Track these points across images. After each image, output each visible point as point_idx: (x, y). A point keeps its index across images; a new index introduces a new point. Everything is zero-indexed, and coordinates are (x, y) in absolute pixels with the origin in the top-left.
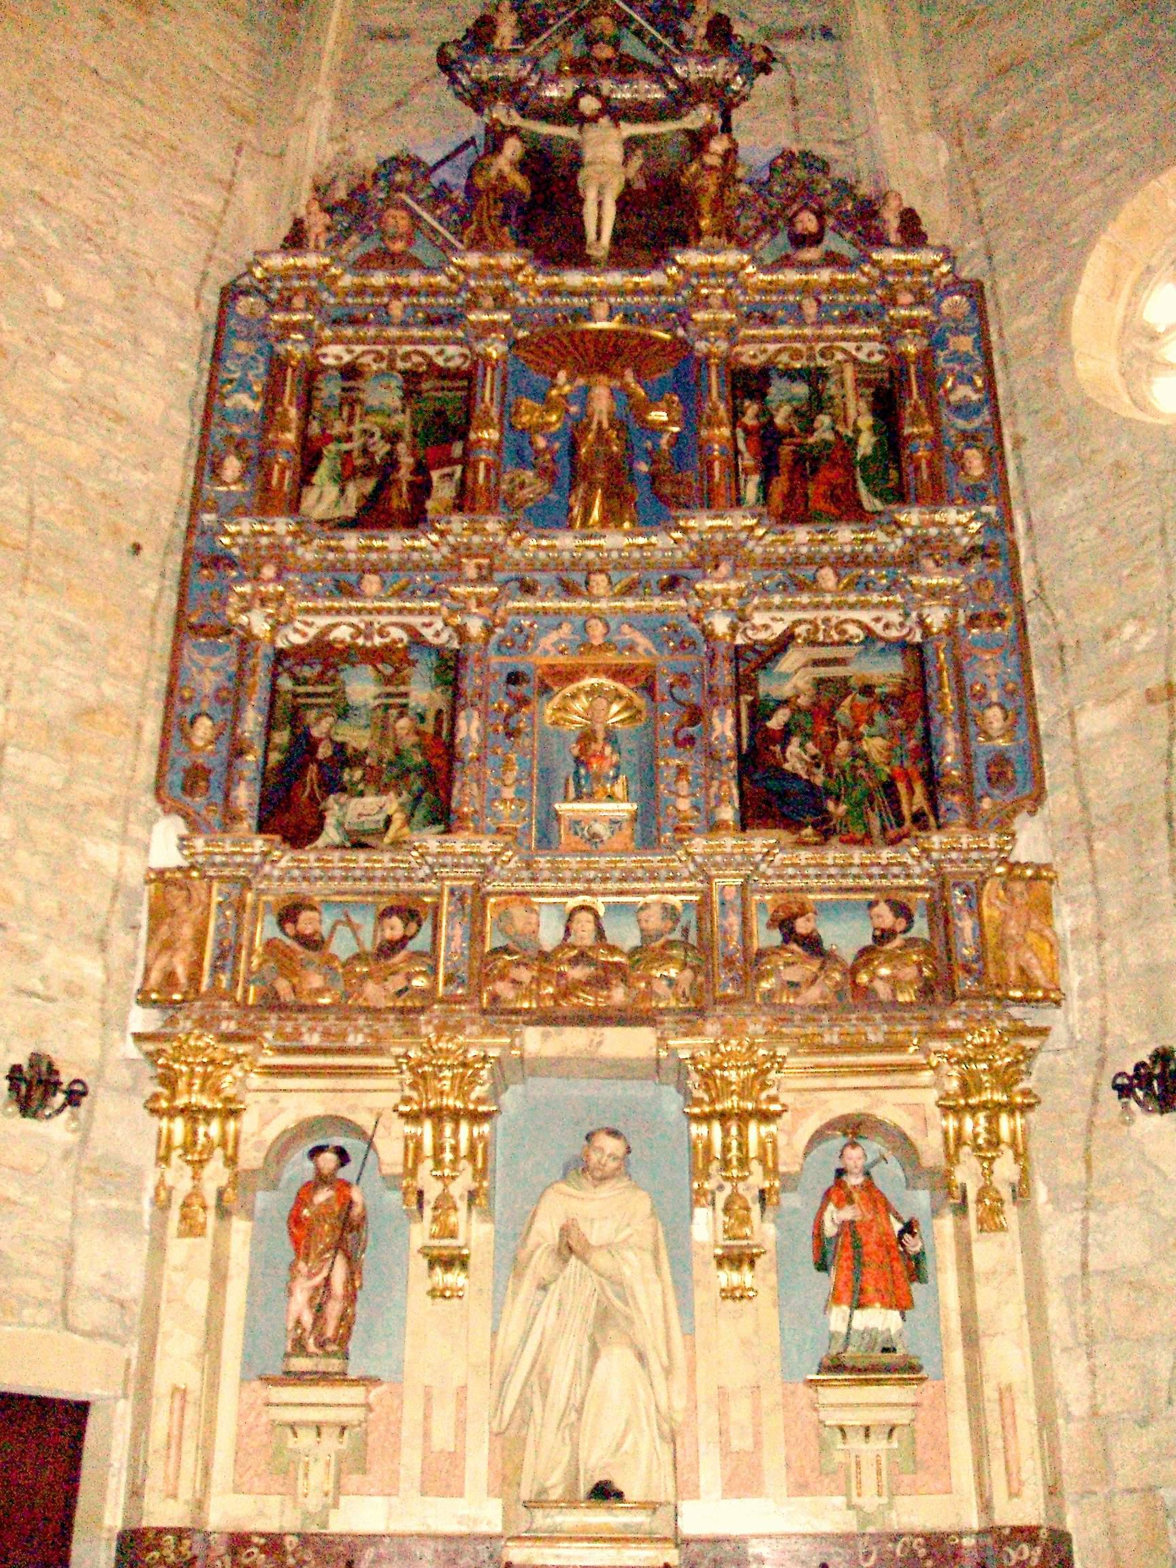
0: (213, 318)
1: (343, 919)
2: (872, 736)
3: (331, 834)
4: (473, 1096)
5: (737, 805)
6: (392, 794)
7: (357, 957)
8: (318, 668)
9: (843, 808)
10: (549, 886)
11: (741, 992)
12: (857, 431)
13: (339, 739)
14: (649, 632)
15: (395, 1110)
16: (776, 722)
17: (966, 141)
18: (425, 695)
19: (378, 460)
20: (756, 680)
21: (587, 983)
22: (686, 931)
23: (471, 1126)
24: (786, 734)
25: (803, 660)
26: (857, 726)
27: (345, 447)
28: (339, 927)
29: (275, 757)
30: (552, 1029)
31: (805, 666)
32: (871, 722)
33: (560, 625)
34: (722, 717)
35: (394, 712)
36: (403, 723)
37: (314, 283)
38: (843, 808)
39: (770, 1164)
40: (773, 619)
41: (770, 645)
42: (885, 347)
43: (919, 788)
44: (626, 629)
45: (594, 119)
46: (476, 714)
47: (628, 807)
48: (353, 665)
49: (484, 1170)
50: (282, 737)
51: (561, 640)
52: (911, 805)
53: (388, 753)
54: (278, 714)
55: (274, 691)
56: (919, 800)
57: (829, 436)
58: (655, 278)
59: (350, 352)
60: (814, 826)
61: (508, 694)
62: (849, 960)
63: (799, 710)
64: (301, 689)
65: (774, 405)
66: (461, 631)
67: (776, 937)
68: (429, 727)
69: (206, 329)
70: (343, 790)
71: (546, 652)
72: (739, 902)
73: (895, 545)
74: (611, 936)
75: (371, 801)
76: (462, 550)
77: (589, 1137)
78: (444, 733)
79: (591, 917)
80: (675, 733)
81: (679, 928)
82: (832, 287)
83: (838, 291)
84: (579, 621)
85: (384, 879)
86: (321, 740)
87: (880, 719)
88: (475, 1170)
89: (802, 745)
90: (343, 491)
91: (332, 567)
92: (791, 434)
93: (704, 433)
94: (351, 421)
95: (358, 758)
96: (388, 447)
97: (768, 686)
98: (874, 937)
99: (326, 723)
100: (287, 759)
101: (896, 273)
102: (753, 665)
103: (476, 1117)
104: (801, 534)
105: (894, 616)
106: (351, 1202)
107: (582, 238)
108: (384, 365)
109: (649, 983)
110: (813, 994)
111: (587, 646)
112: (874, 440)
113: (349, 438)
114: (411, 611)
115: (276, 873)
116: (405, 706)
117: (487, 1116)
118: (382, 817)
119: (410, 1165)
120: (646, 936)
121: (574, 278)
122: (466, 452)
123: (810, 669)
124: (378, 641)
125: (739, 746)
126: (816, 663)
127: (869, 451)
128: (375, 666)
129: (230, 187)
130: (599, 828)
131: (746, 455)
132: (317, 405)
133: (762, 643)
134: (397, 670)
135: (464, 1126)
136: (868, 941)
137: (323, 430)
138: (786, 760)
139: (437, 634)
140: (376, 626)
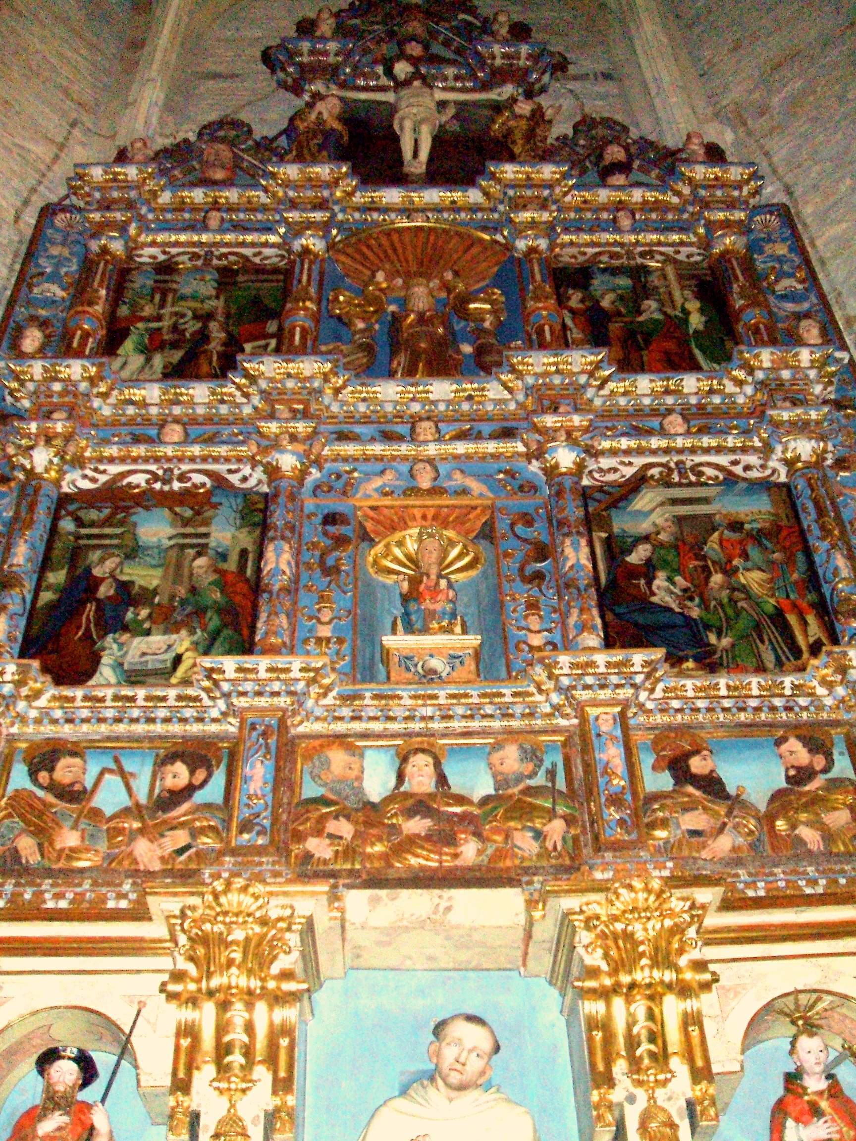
0: (29, 232)
1: (113, 766)
2: (748, 570)
3: (106, 672)
4: (275, 969)
5: (602, 634)
6: (184, 632)
7: (125, 812)
8: (107, 511)
9: (726, 642)
10: (377, 727)
11: (634, 836)
12: (686, 313)
13: (125, 578)
14: (486, 478)
15: (162, 991)
16: (635, 558)
17: (749, 122)
18: (229, 535)
19: (188, 335)
20: (609, 517)
21: (428, 838)
22: (552, 774)
23: (271, 1008)
24: (648, 570)
25: (659, 499)
26: (730, 561)
27: (155, 325)
28: (107, 776)
29: (46, 597)
30: (383, 893)
31: (662, 504)
32: (745, 556)
33: (383, 472)
34: (576, 548)
35: (191, 552)
36: (201, 561)
37: (133, 194)
38: (726, 642)
39: (700, 1063)
40: (622, 463)
41: (621, 486)
42: (702, 251)
43: (811, 619)
44: (458, 476)
45: (407, 83)
46: (286, 547)
47: (473, 640)
48: (147, 508)
49: (290, 1079)
50: (57, 577)
51: (385, 485)
52: (806, 634)
53: (182, 591)
54: (56, 553)
55: (54, 530)
56: (815, 629)
57: (658, 316)
58: (474, 196)
59: (164, 253)
60: (696, 659)
61: (325, 534)
62: (762, 807)
63: (662, 545)
64: (84, 531)
65: (598, 293)
66: (273, 472)
67: (664, 781)
68: (232, 565)
69: (20, 242)
70: (125, 628)
71: (368, 497)
72: (618, 733)
73: (744, 395)
74: (457, 784)
75: (157, 640)
76: (275, 396)
77: (439, 1029)
78: (249, 572)
79: (430, 760)
80: (522, 569)
81: (542, 773)
82: (645, 206)
83: (652, 210)
84: (404, 468)
85: (167, 720)
86: (102, 580)
87: (754, 552)
88: (275, 1080)
89: (670, 579)
90: (148, 360)
91: (132, 421)
92: (619, 314)
93: (531, 304)
94: (162, 305)
95: (145, 597)
96: (199, 325)
97: (621, 523)
98: (788, 778)
99: (110, 564)
100: (59, 600)
101: (705, 187)
102: (603, 506)
103: (278, 999)
104: (645, 383)
105: (753, 459)
106: (92, 1128)
107: (399, 160)
108: (199, 263)
109: (507, 837)
110: (724, 844)
111: (413, 491)
112: (703, 319)
113: (159, 318)
114: (216, 460)
115: (33, 714)
116: (206, 546)
117: (293, 997)
118: (170, 656)
119: (181, 1074)
120: (501, 782)
121: (392, 196)
122: (281, 328)
123: (671, 508)
124: (176, 485)
125: (596, 578)
126: (675, 502)
127: (701, 327)
128: (171, 509)
129: (62, 147)
130: (436, 663)
131: (575, 330)
132: (128, 294)
133: (611, 484)
134: (198, 513)
135: (261, 1007)
136: (781, 783)
137: (133, 312)
138: (653, 594)
139: (245, 479)
140: (176, 472)
